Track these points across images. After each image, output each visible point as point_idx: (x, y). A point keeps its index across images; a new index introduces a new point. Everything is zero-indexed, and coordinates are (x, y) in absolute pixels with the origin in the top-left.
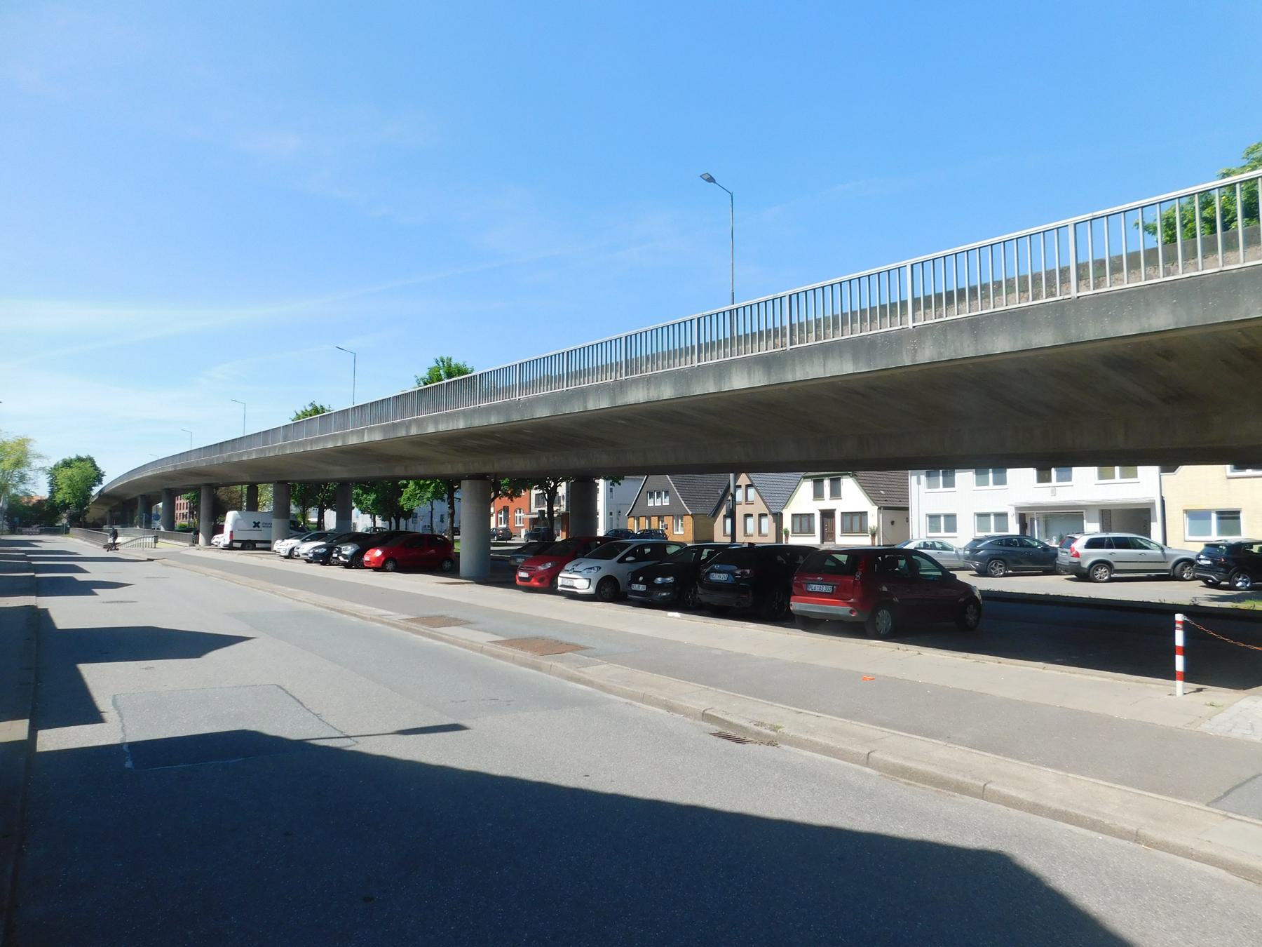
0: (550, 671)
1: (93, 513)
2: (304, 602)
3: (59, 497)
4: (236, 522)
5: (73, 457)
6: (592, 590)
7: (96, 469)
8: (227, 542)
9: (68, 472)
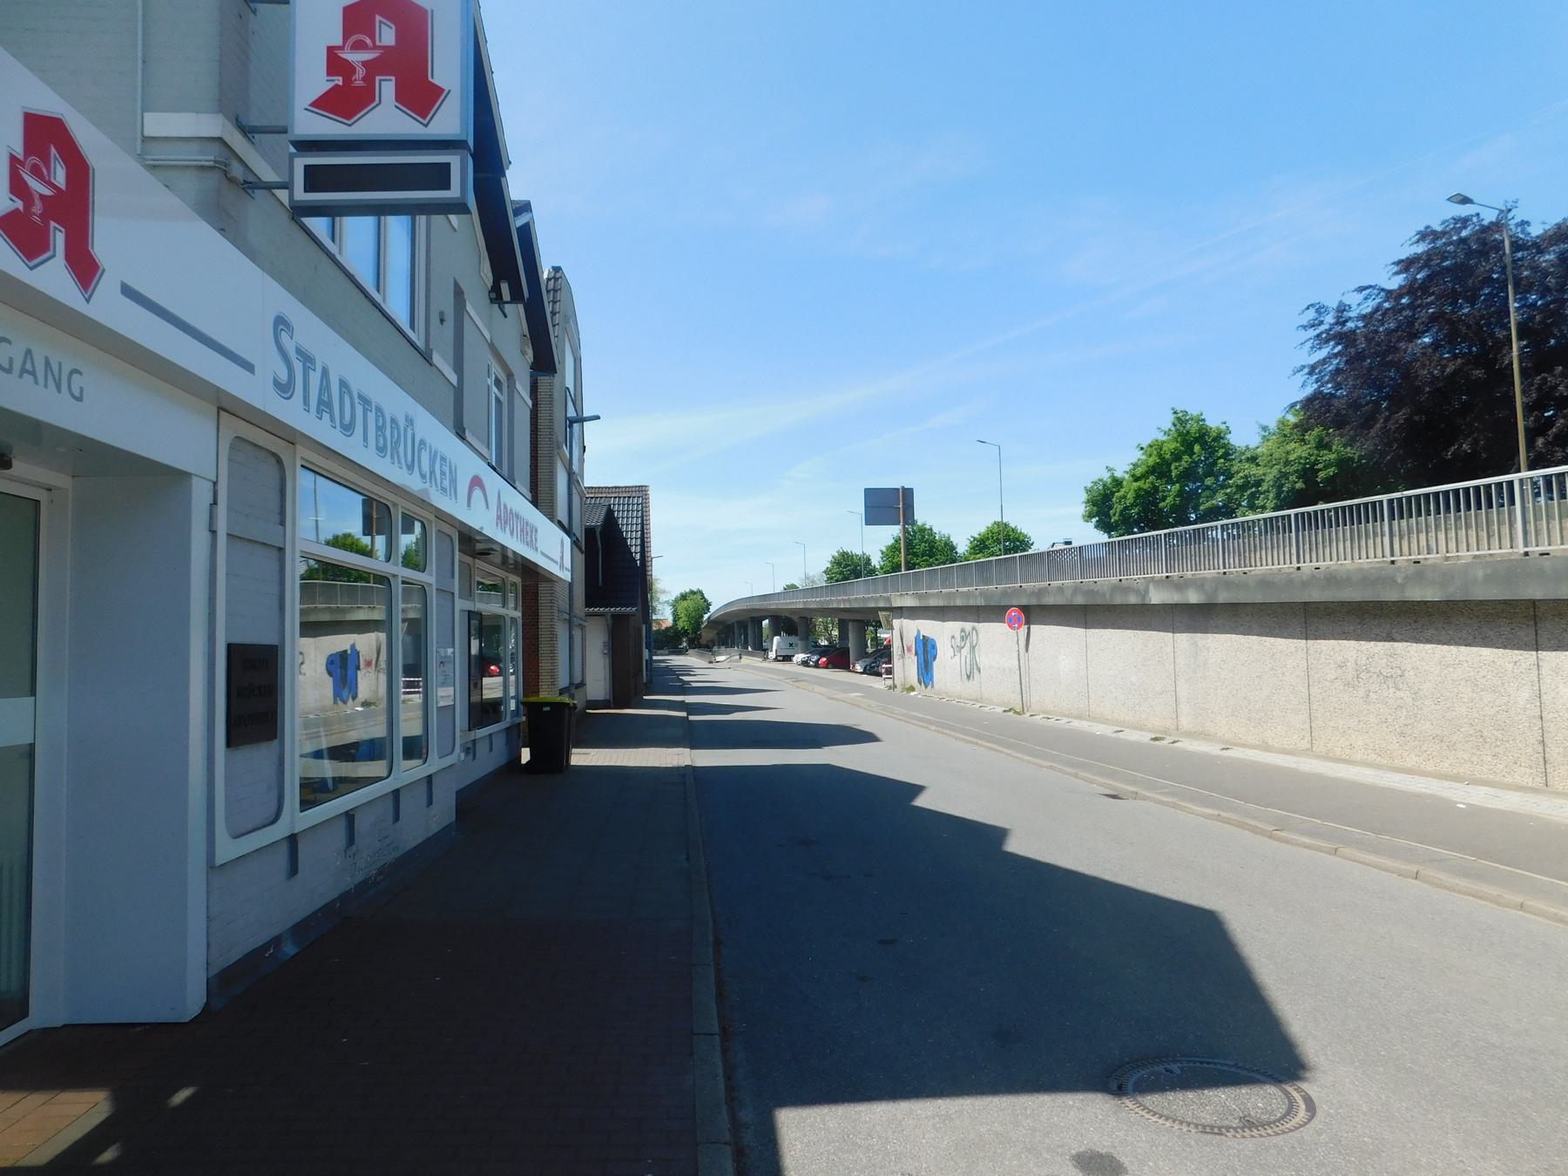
0: (1100, 785)
1: (706, 636)
2: (864, 709)
3: (681, 624)
4: (778, 643)
5: (688, 591)
6: (862, 670)
7: (706, 601)
8: (774, 657)
9: (685, 604)
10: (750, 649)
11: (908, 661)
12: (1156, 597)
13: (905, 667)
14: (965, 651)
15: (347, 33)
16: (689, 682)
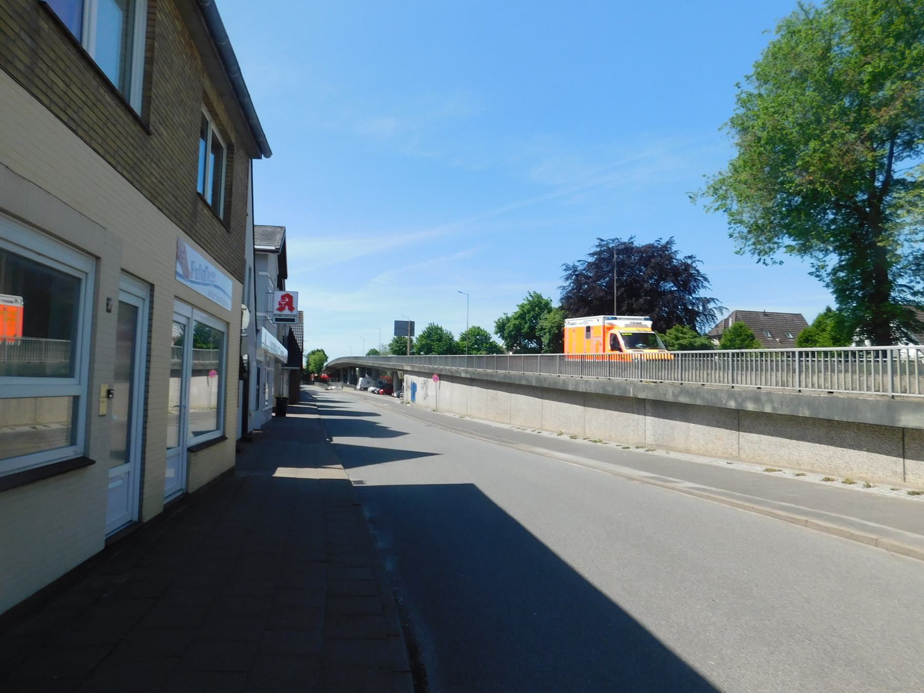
3: (311, 368)
4: (362, 381)
5: (316, 349)
7: (325, 355)
9: (313, 357)
10: (348, 383)
11: (408, 392)
12: (463, 375)
13: (407, 394)
14: (425, 389)
15: (282, 299)
16: (316, 398)
